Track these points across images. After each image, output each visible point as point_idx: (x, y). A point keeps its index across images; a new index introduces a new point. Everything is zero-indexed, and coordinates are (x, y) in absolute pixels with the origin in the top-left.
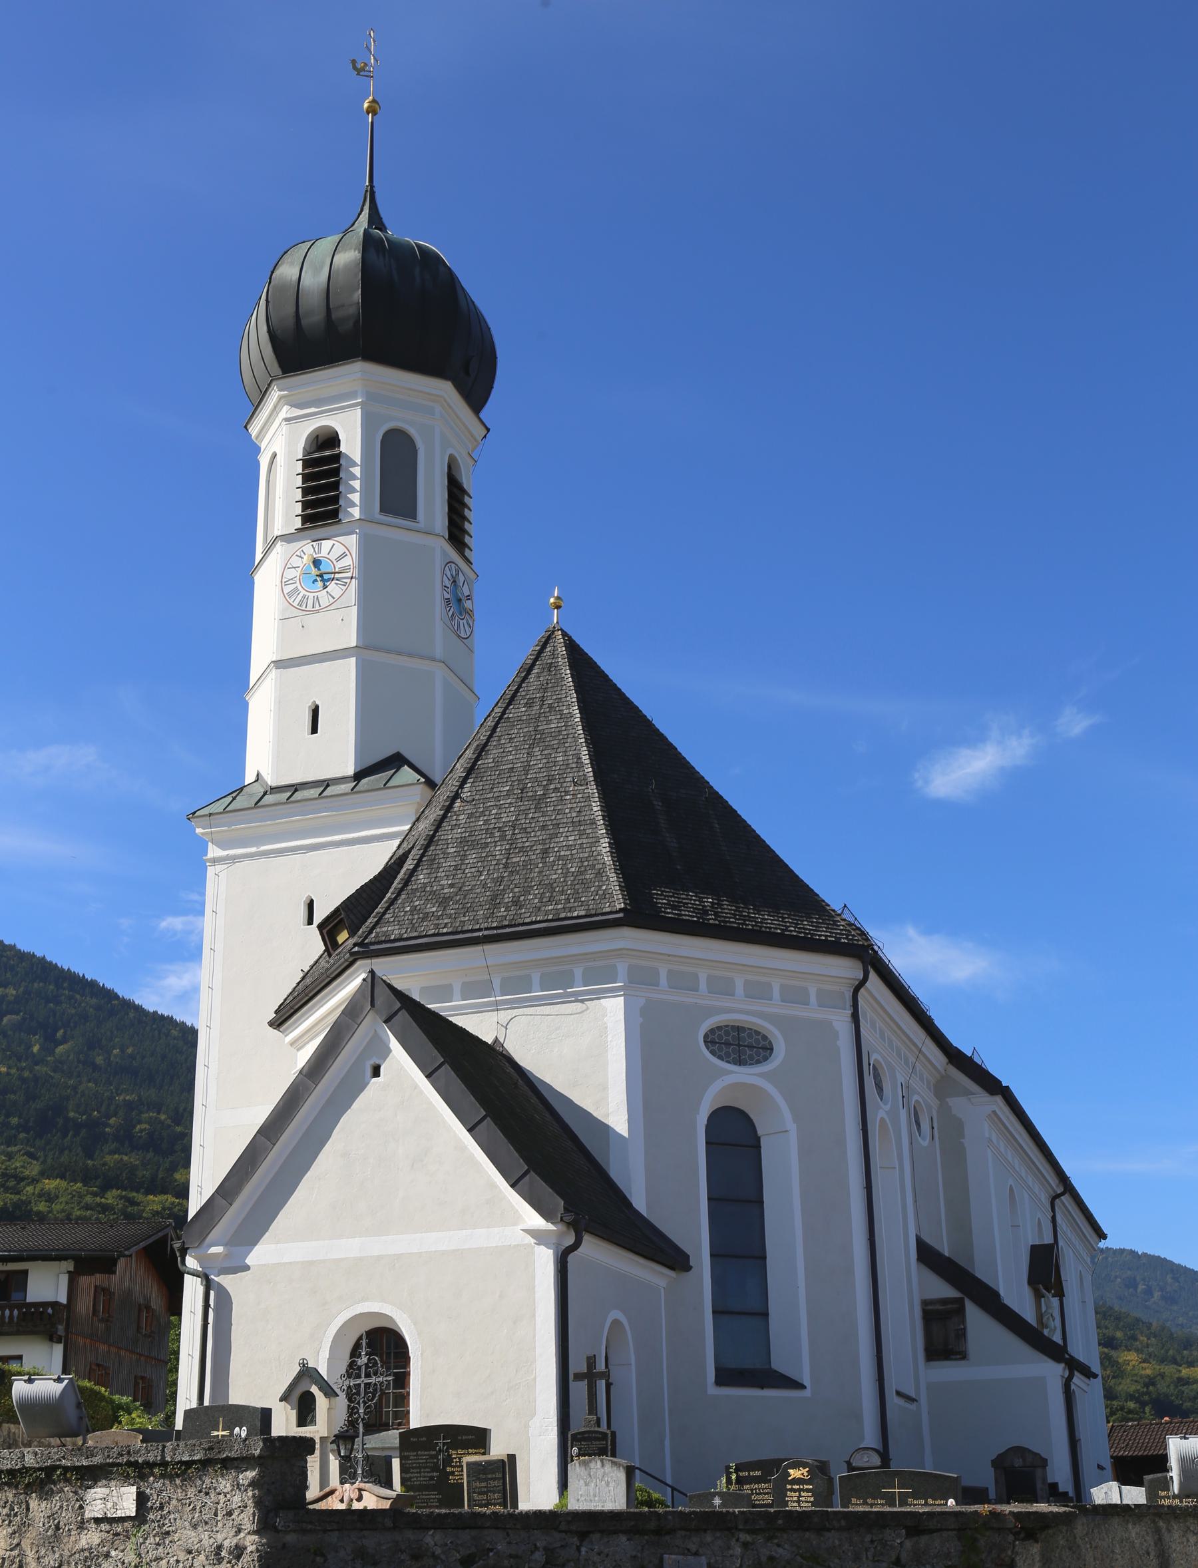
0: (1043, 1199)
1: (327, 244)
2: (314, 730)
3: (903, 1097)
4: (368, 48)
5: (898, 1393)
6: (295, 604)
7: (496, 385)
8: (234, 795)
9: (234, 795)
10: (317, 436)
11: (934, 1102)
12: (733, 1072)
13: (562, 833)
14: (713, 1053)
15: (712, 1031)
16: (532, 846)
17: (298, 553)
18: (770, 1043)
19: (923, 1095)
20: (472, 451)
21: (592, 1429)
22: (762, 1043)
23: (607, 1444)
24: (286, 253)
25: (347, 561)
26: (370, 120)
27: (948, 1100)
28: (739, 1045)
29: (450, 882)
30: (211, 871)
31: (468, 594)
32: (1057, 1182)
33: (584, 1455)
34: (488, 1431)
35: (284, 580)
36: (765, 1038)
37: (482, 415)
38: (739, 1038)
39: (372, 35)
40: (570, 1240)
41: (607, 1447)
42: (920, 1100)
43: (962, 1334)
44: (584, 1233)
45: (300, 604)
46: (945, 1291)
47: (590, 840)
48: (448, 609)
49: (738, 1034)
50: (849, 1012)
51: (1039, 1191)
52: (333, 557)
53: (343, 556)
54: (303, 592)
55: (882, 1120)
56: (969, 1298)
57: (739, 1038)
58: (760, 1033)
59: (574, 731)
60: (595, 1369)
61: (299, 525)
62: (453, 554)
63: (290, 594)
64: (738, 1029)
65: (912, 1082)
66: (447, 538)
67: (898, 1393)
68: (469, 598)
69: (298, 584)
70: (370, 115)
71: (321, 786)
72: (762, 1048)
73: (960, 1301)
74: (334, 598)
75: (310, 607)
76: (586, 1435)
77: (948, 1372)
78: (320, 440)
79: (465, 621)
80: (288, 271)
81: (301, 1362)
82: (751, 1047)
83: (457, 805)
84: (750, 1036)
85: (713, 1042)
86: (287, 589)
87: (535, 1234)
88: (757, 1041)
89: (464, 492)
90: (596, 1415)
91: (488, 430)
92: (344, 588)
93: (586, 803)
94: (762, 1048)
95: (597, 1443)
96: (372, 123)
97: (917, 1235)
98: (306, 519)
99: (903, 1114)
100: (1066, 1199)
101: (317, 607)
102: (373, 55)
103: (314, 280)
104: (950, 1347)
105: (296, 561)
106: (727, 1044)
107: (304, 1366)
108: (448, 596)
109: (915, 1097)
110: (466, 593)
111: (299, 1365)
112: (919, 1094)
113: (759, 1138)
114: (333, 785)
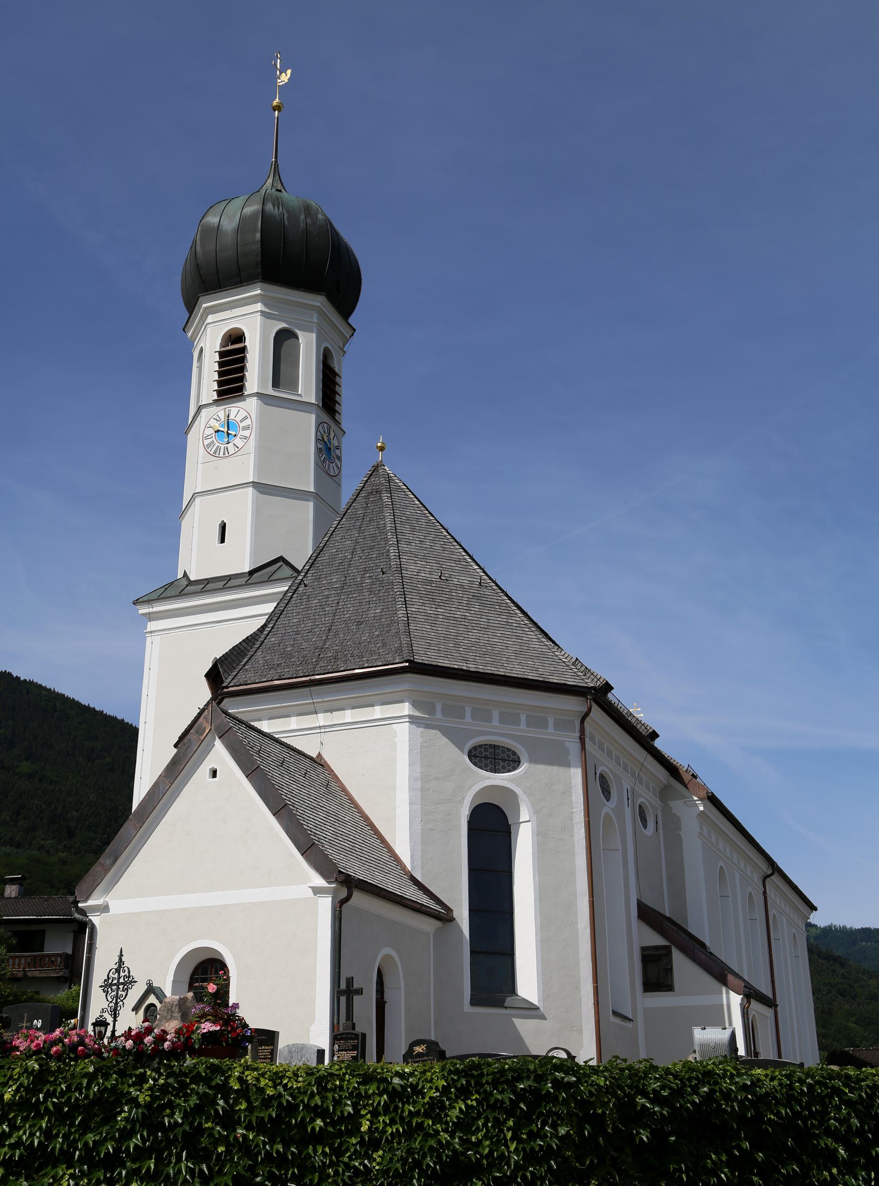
0: (755, 879)
1: (238, 202)
2: (222, 540)
3: (628, 799)
4: (275, 65)
5: (615, 1013)
6: (212, 453)
7: (360, 299)
8: (166, 587)
9: (166, 587)
10: (230, 335)
11: (656, 801)
12: (488, 778)
13: (372, 607)
14: (475, 764)
15: (475, 748)
16: (350, 617)
17: (214, 417)
18: (518, 757)
19: (648, 798)
20: (344, 346)
21: (349, 1031)
22: (512, 757)
23: (358, 1042)
24: (211, 207)
25: (247, 422)
26: (276, 116)
27: (669, 802)
28: (495, 759)
29: (292, 643)
30: (149, 640)
31: (338, 445)
32: (767, 866)
33: (342, 1050)
34: (276, 1033)
35: (205, 436)
36: (514, 753)
37: (350, 320)
38: (495, 753)
39: (279, 56)
40: (344, 893)
41: (358, 1044)
42: (645, 801)
43: (669, 971)
44: (354, 888)
45: (215, 452)
46: (656, 940)
47: (391, 613)
48: (321, 455)
49: (495, 751)
50: (578, 734)
51: (755, 871)
52: (238, 419)
53: (245, 418)
54: (217, 444)
55: (607, 815)
56: (676, 946)
57: (495, 753)
58: (511, 750)
59: (386, 536)
60: (353, 987)
61: (216, 397)
62: (325, 418)
63: (209, 445)
64: (495, 747)
65: (637, 789)
66: (321, 405)
67: (615, 1013)
68: (338, 448)
69: (214, 439)
70: (277, 112)
71: (224, 580)
72: (512, 761)
73: (668, 949)
74: (238, 448)
75: (221, 455)
76: (344, 1036)
77: (659, 1000)
78: (233, 338)
79: (334, 464)
80: (212, 220)
81: (148, 982)
82: (503, 760)
83: (301, 589)
84: (503, 752)
85: (476, 756)
86: (207, 442)
87: (317, 891)
88: (508, 756)
89: (335, 374)
90: (352, 1021)
91: (355, 330)
92: (245, 441)
93: (390, 587)
94: (512, 761)
95: (352, 1041)
96: (278, 117)
97: (638, 900)
98: (220, 393)
99: (628, 812)
100: (775, 878)
101: (227, 455)
102: (277, 69)
103: (229, 224)
104: (661, 982)
105: (213, 423)
106: (486, 758)
107: (150, 985)
108: (321, 446)
109: (641, 800)
110: (336, 444)
111: (147, 984)
112: (644, 797)
113: (510, 826)
114: (235, 579)
